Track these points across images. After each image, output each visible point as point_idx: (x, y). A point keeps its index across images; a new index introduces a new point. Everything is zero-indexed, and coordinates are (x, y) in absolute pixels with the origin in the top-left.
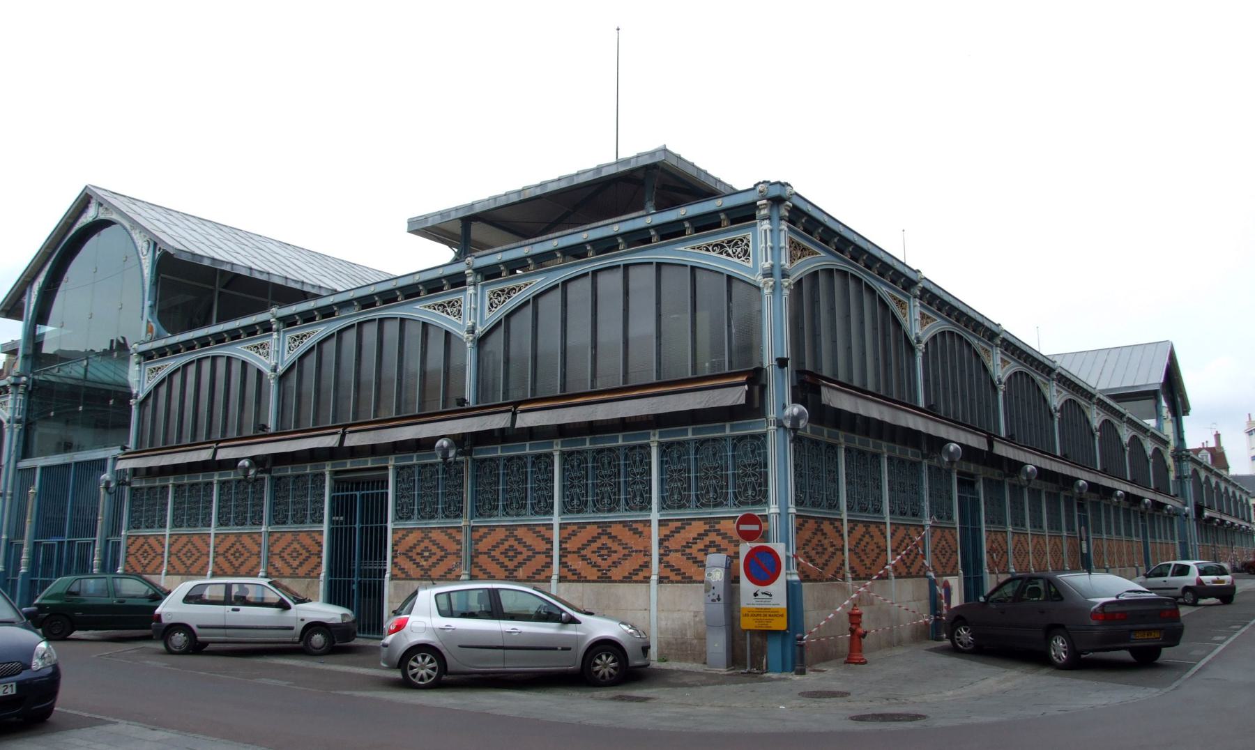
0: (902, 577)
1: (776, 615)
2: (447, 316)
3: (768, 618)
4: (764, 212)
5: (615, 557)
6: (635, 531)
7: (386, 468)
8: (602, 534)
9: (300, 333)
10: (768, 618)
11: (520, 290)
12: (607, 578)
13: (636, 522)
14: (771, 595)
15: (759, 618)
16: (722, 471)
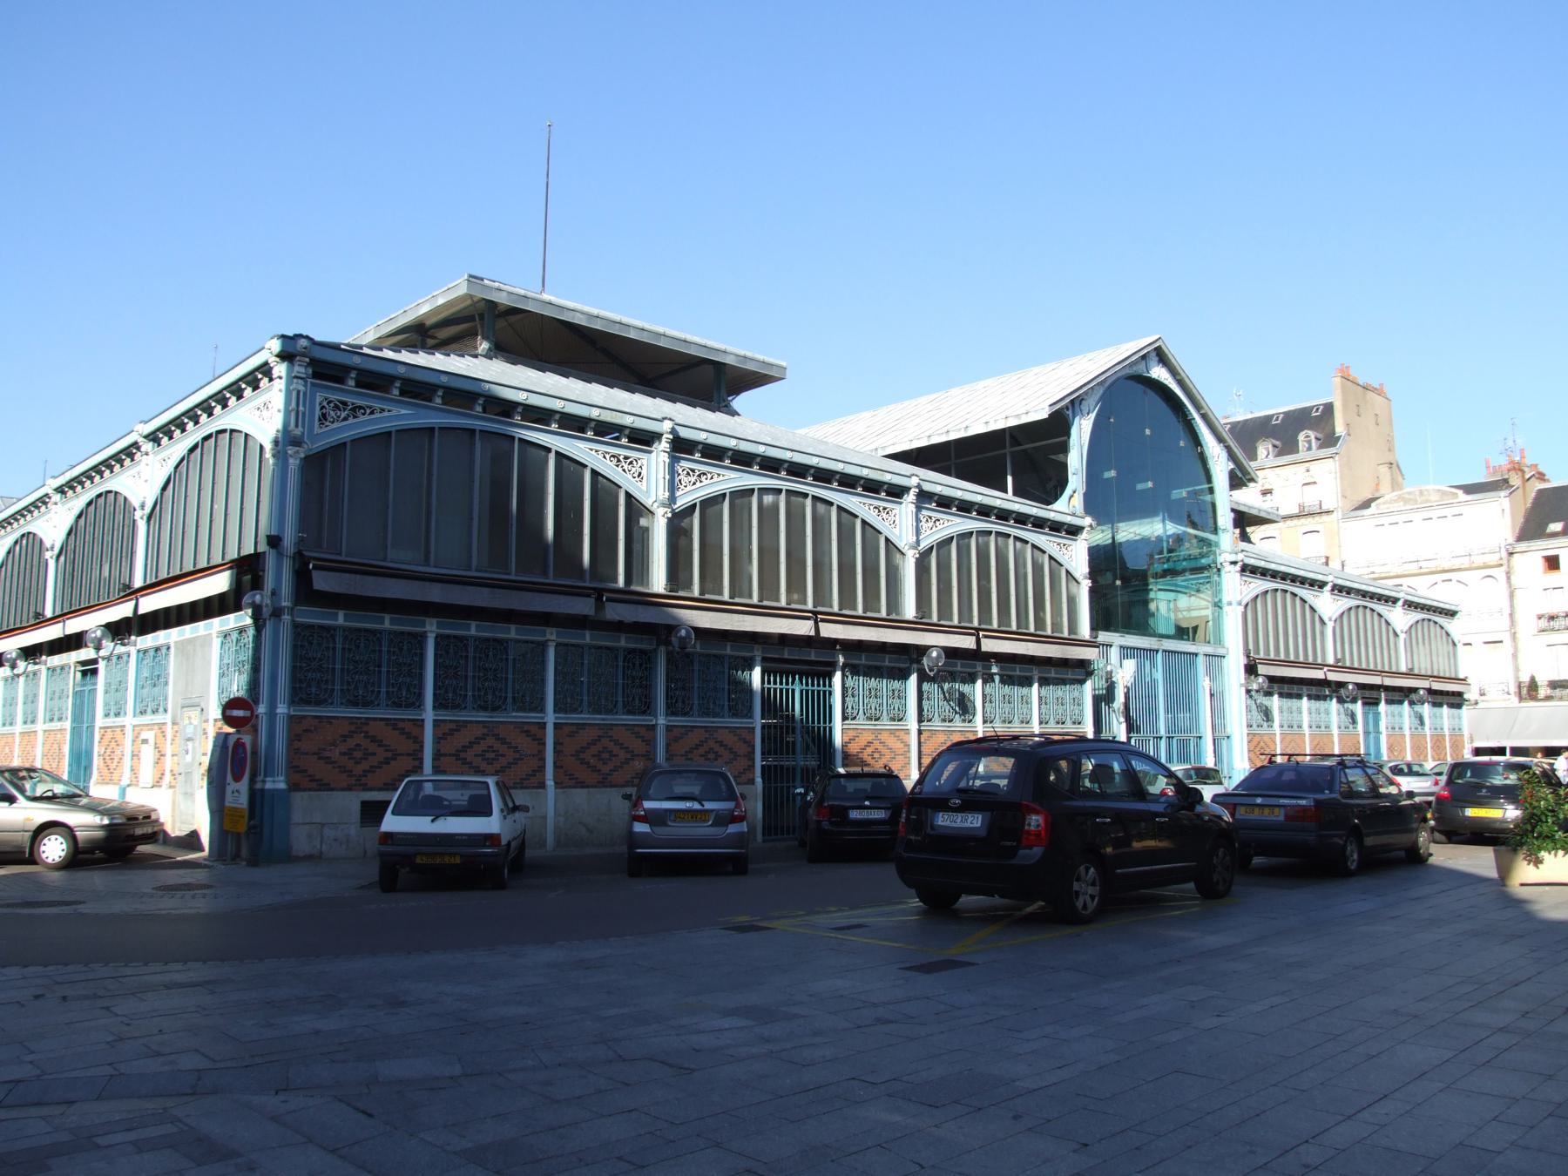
11: (372, 413)
13: (403, 720)
16: (348, 669)
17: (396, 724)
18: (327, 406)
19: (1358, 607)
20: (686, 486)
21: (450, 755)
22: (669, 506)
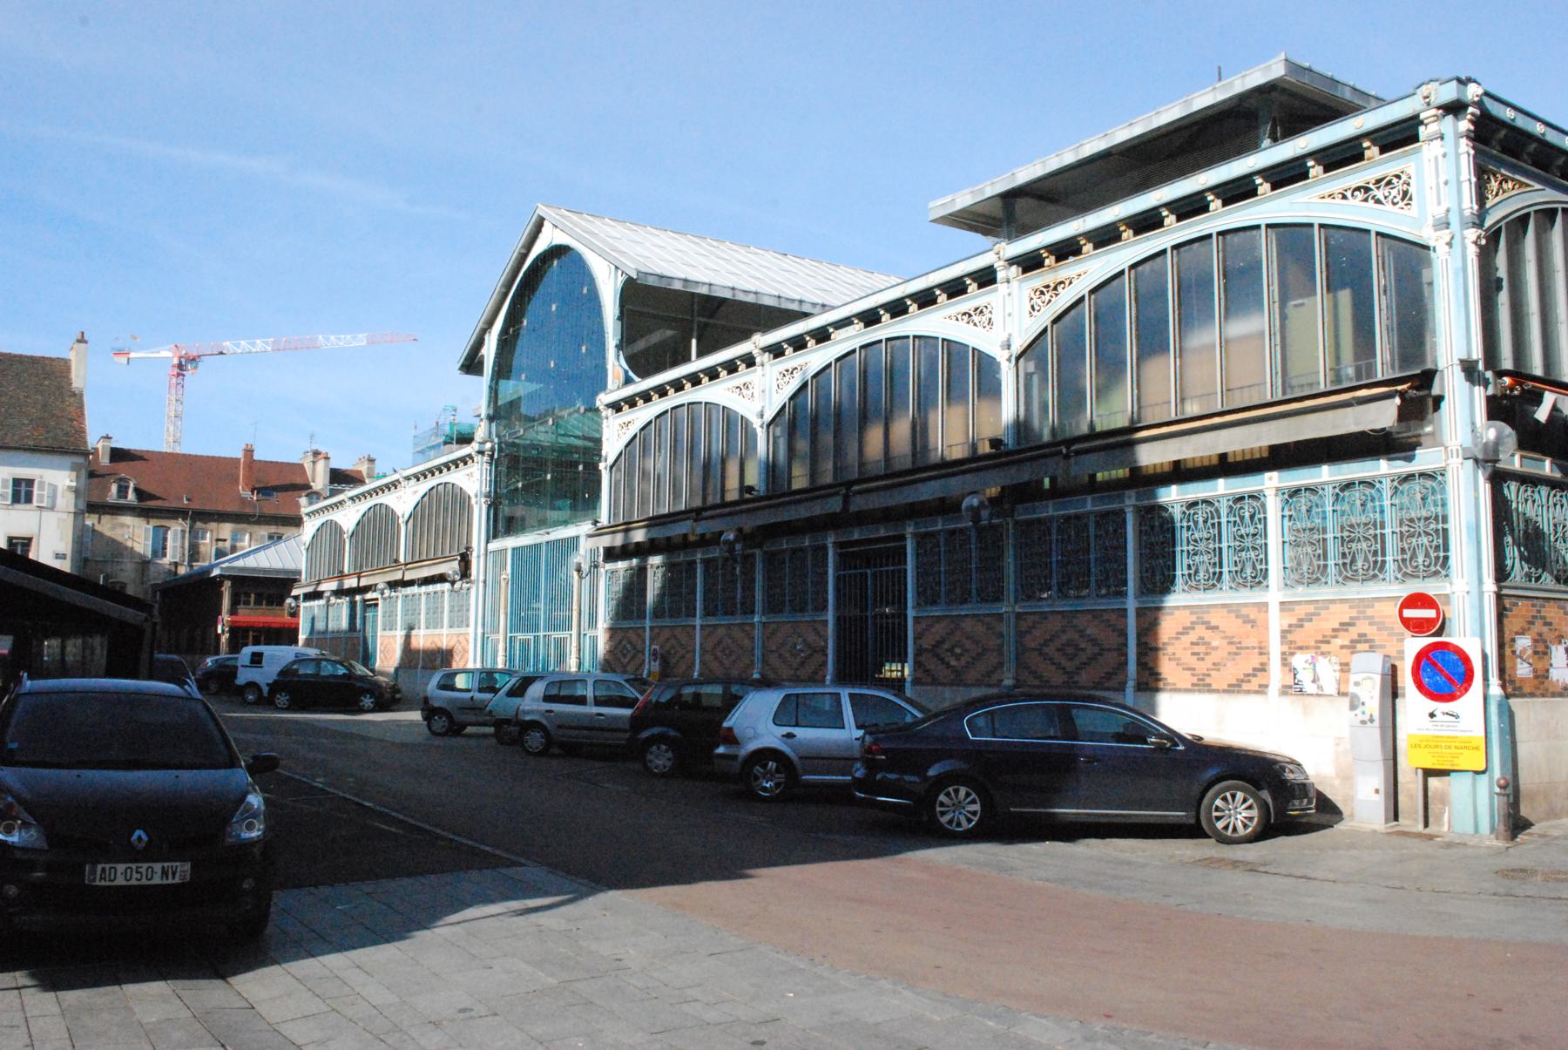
1: (1466, 747)
2: (1377, 206)
5: (1215, 657)
6: (1247, 621)
7: (902, 538)
8: (1198, 623)
11: (1071, 283)
12: (1204, 685)
13: (1246, 605)
14: (1457, 717)
15: (1439, 750)
17: (1239, 611)
18: (1401, 182)
21: (1247, 648)
22: (1480, 225)
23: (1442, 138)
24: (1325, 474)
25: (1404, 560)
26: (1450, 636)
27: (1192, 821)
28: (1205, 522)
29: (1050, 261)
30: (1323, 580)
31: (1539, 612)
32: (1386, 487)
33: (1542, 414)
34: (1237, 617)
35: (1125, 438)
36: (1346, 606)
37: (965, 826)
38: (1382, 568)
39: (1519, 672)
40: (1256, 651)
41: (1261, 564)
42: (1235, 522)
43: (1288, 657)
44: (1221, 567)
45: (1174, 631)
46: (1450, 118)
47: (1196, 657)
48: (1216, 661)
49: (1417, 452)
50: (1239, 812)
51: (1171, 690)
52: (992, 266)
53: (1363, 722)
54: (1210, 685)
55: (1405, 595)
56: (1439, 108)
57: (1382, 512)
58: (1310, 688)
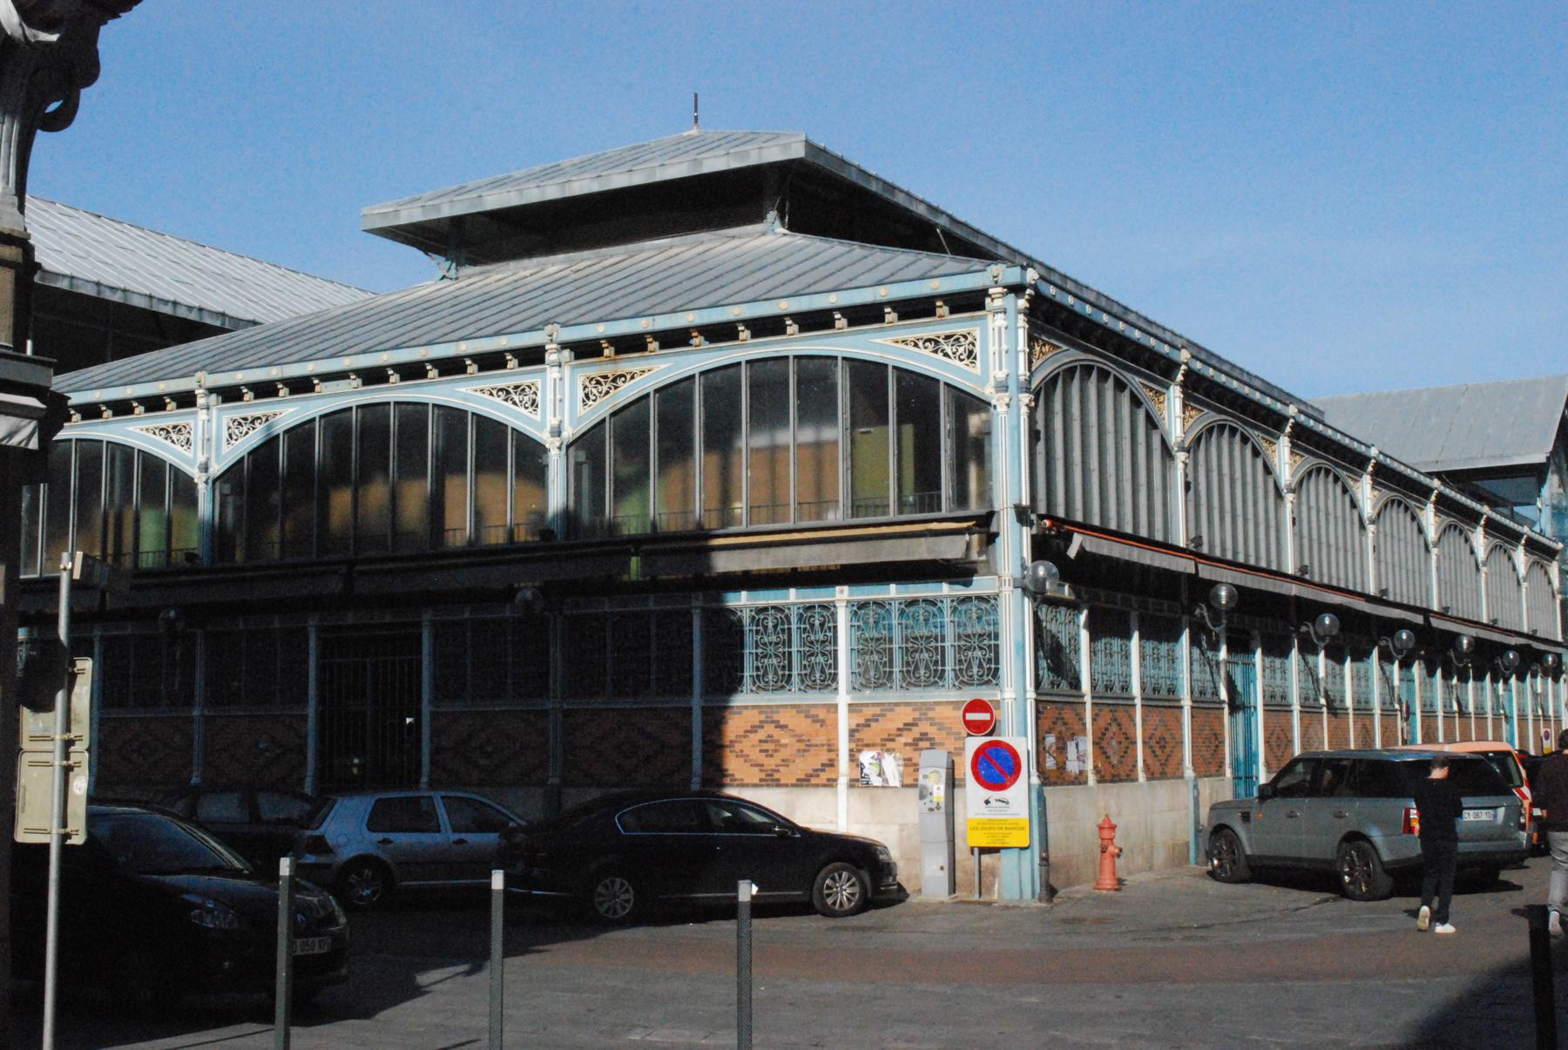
0: (1106, 781)
1: (1014, 828)
2: (946, 359)
3: (1004, 831)
4: (998, 303)
5: (784, 753)
6: (816, 720)
7: (419, 625)
8: (767, 722)
9: (610, 370)
10: (1004, 831)
11: (632, 378)
12: (773, 780)
13: (815, 706)
14: (1007, 803)
15: (992, 831)
19: (1087, 370)
20: (594, 401)
21: (817, 746)
23: (1005, 313)
24: (893, 592)
25: (961, 670)
26: (999, 735)
27: (806, 899)
28: (775, 627)
29: (609, 352)
30: (889, 685)
31: (1059, 714)
32: (947, 607)
33: (1072, 552)
34: (807, 717)
35: (699, 544)
36: (910, 709)
37: (621, 913)
38: (942, 677)
39: (1048, 765)
40: (825, 748)
41: (830, 668)
42: (805, 629)
43: (857, 754)
44: (790, 670)
45: (743, 729)
46: (1012, 296)
47: (764, 754)
48: (785, 758)
49: (974, 578)
50: (844, 890)
51: (738, 786)
52: (544, 347)
53: (931, 810)
54: (778, 780)
55: (968, 699)
56: (1004, 287)
57: (942, 627)
58: (876, 781)
